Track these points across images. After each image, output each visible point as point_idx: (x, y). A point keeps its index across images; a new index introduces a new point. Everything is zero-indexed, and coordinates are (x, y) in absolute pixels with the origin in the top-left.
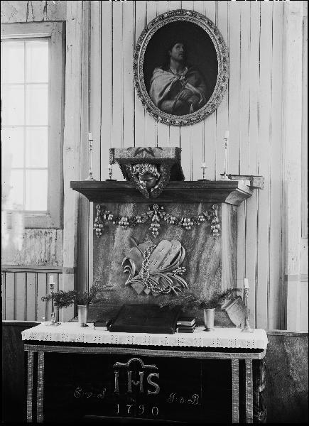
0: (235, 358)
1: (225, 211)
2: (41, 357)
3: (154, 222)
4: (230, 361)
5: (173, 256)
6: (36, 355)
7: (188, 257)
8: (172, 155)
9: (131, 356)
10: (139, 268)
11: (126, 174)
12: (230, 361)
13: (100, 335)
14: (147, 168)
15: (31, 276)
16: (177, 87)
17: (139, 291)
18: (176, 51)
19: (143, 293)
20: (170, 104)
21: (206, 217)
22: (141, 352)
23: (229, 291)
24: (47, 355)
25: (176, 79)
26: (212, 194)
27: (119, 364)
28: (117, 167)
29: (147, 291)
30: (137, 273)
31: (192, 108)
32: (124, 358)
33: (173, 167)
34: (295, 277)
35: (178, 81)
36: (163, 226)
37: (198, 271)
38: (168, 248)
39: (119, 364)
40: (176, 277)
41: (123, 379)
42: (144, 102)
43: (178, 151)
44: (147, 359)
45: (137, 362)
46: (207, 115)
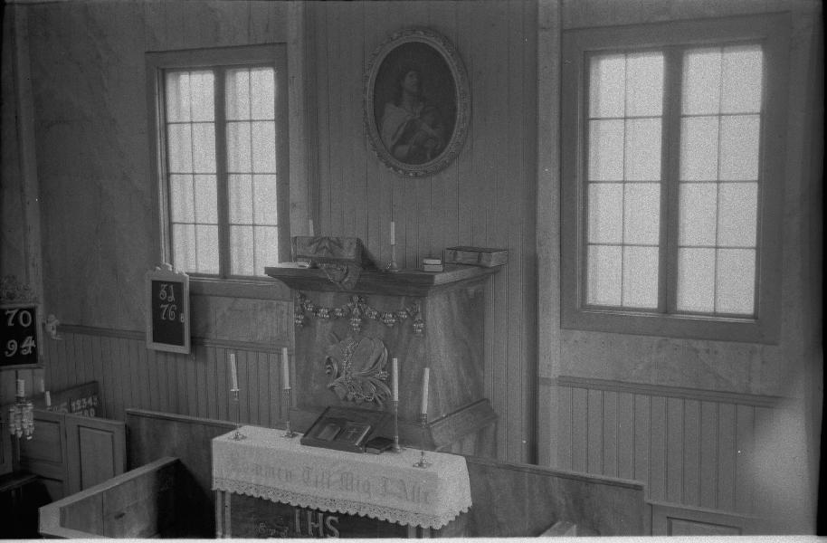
3: (354, 316)
15: (262, 356)
17: (341, 396)
18: (410, 82)
21: (408, 314)
25: (408, 118)
29: (350, 397)
31: (428, 155)
34: (548, 381)
36: (365, 321)
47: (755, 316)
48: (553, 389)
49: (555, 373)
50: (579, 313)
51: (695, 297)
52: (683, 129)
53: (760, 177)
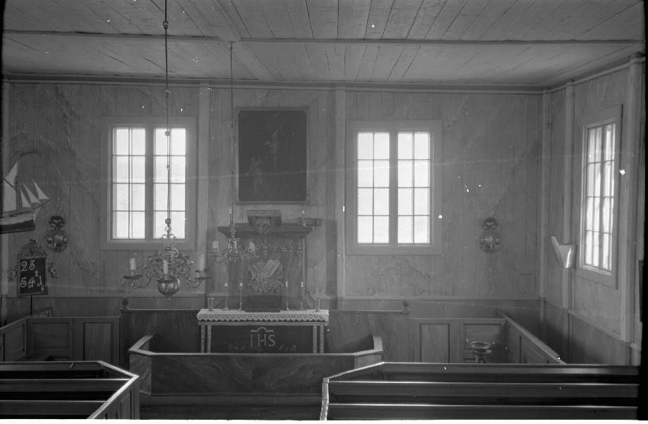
0: (315, 325)
1: (304, 239)
2: (209, 328)
4: (312, 326)
5: (275, 269)
7: (284, 269)
12: (312, 326)
17: (256, 290)
19: (259, 291)
24: (312, 352)
27: (252, 331)
29: (261, 290)
32: (256, 327)
33: (278, 221)
38: (273, 264)
39: (252, 331)
41: (255, 339)
44: (269, 328)
45: (263, 330)
47: (431, 244)
53: (186, 153)
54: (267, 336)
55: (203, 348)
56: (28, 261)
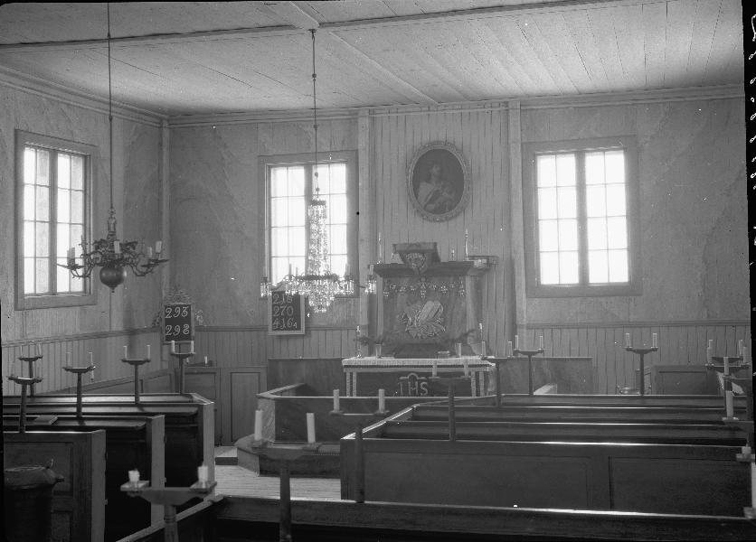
1: (469, 282)
2: (354, 375)
6: (351, 374)
8: (431, 247)
9: (410, 372)
10: (413, 319)
11: (403, 259)
13: (390, 361)
14: (416, 255)
16: (436, 194)
18: (435, 170)
19: (417, 336)
20: (432, 207)
22: (413, 369)
23: (472, 331)
24: (359, 374)
26: (458, 269)
27: (402, 378)
28: (397, 255)
29: (419, 335)
30: (412, 324)
32: (406, 374)
33: (435, 257)
34: (522, 326)
35: (438, 191)
36: (429, 291)
37: (451, 322)
38: (429, 308)
39: (402, 378)
40: (438, 325)
42: (414, 206)
43: (435, 244)
44: (420, 374)
46: (458, 214)
48: (525, 330)
49: (525, 322)
50: (536, 290)
51: (597, 277)
52: (626, 176)
53: (627, 213)
54: (419, 384)
55: (348, 390)
56: (173, 308)
